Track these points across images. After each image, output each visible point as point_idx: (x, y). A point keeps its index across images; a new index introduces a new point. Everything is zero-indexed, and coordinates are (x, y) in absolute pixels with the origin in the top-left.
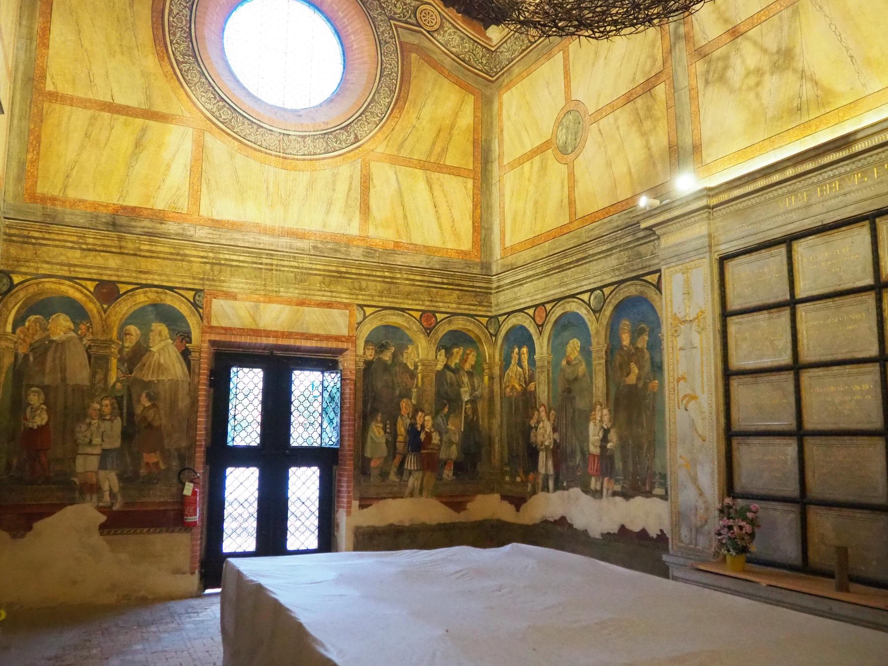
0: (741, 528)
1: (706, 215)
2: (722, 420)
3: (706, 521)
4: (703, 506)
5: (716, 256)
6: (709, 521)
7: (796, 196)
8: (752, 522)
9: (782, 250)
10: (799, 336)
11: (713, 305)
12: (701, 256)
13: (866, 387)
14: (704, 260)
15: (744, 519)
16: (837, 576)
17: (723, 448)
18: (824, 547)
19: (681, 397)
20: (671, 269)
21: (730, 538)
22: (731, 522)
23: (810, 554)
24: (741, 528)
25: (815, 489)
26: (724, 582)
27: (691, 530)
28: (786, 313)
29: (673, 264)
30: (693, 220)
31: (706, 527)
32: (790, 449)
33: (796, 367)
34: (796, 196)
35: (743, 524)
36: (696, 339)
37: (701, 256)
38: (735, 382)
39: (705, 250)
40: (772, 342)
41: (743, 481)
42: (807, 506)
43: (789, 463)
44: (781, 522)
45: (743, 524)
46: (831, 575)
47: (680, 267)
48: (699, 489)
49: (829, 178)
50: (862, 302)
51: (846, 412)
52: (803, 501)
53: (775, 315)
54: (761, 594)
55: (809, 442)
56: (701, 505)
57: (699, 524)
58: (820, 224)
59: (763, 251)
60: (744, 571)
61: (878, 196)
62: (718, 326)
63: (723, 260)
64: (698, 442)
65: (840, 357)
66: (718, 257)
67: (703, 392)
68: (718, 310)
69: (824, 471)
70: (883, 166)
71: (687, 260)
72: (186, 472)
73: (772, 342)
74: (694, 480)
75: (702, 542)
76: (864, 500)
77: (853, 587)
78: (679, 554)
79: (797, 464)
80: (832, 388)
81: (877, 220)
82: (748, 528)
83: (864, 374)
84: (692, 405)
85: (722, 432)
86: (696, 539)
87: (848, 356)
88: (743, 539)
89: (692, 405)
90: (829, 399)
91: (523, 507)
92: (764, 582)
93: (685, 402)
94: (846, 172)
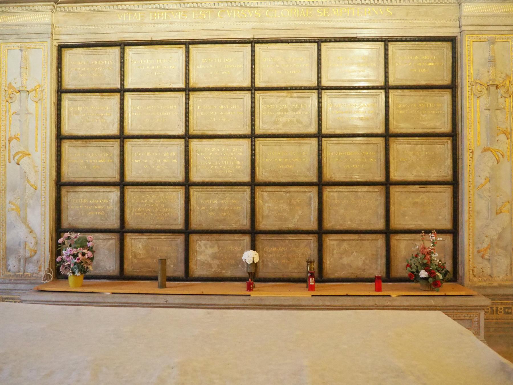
0: (83, 254)
1: (52, 7)
2: (54, 174)
3: (36, 253)
4: (33, 241)
5: (55, 43)
6: (38, 252)
7: (133, 14)
8: (90, 249)
9: (117, 50)
10: (126, 115)
11: (51, 82)
12: (42, 40)
13: (173, 154)
14: (45, 44)
15: (84, 247)
16: (159, 278)
17: (54, 195)
18: (136, 261)
19: (13, 153)
20: (9, 45)
21: (75, 263)
22: (75, 251)
23: (125, 266)
24: (83, 254)
25: (131, 222)
26: (149, 299)
27: (19, 261)
28: (116, 97)
29: (11, 41)
30: (36, 8)
31: (35, 258)
32: (114, 194)
33: (122, 137)
34: (133, 14)
35: (85, 251)
36: (32, 107)
37: (42, 40)
38: (66, 145)
39: (47, 36)
40: (102, 117)
41: (70, 219)
42: (125, 234)
43: (111, 205)
44: (105, 249)
45: (85, 251)
46: (155, 279)
47: (19, 45)
48: (30, 228)
49: (160, 9)
50: (175, 98)
51: (158, 170)
52: (122, 231)
53: (106, 98)
54: (106, 300)
55: (129, 192)
56: (31, 240)
57: (28, 255)
58: (150, 39)
59: (99, 48)
60: (83, 286)
61: (193, 31)
62: (54, 99)
63: (61, 48)
64: (30, 191)
65: (156, 133)
66: (57, 45)
67: (36, 151)
68: (54, 87)
69: (139, 209)
70: (199, 12)
71: (28, 40)
72: (490, 152)
73: (102, 117)
74: (25, 221)
75: (31, 269)
76: (167, 227)
77: (168, 283)
78: (7, 281)
79: (118, 205)
80: (149, 154)
81: (190, 46)
82: (89, 254)
83: (173, 145)
84: (24, 161)
85: (53, 183)
86: (24, 267)
87: (163, 133)
88: (86, 262)
89: (24, 161)
90: (146, 161)
91: (164, 258)
92: (394, 294)
93: (16, 158)
94: (173, 9)
